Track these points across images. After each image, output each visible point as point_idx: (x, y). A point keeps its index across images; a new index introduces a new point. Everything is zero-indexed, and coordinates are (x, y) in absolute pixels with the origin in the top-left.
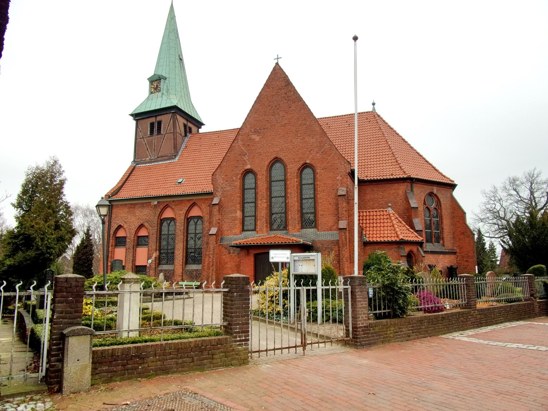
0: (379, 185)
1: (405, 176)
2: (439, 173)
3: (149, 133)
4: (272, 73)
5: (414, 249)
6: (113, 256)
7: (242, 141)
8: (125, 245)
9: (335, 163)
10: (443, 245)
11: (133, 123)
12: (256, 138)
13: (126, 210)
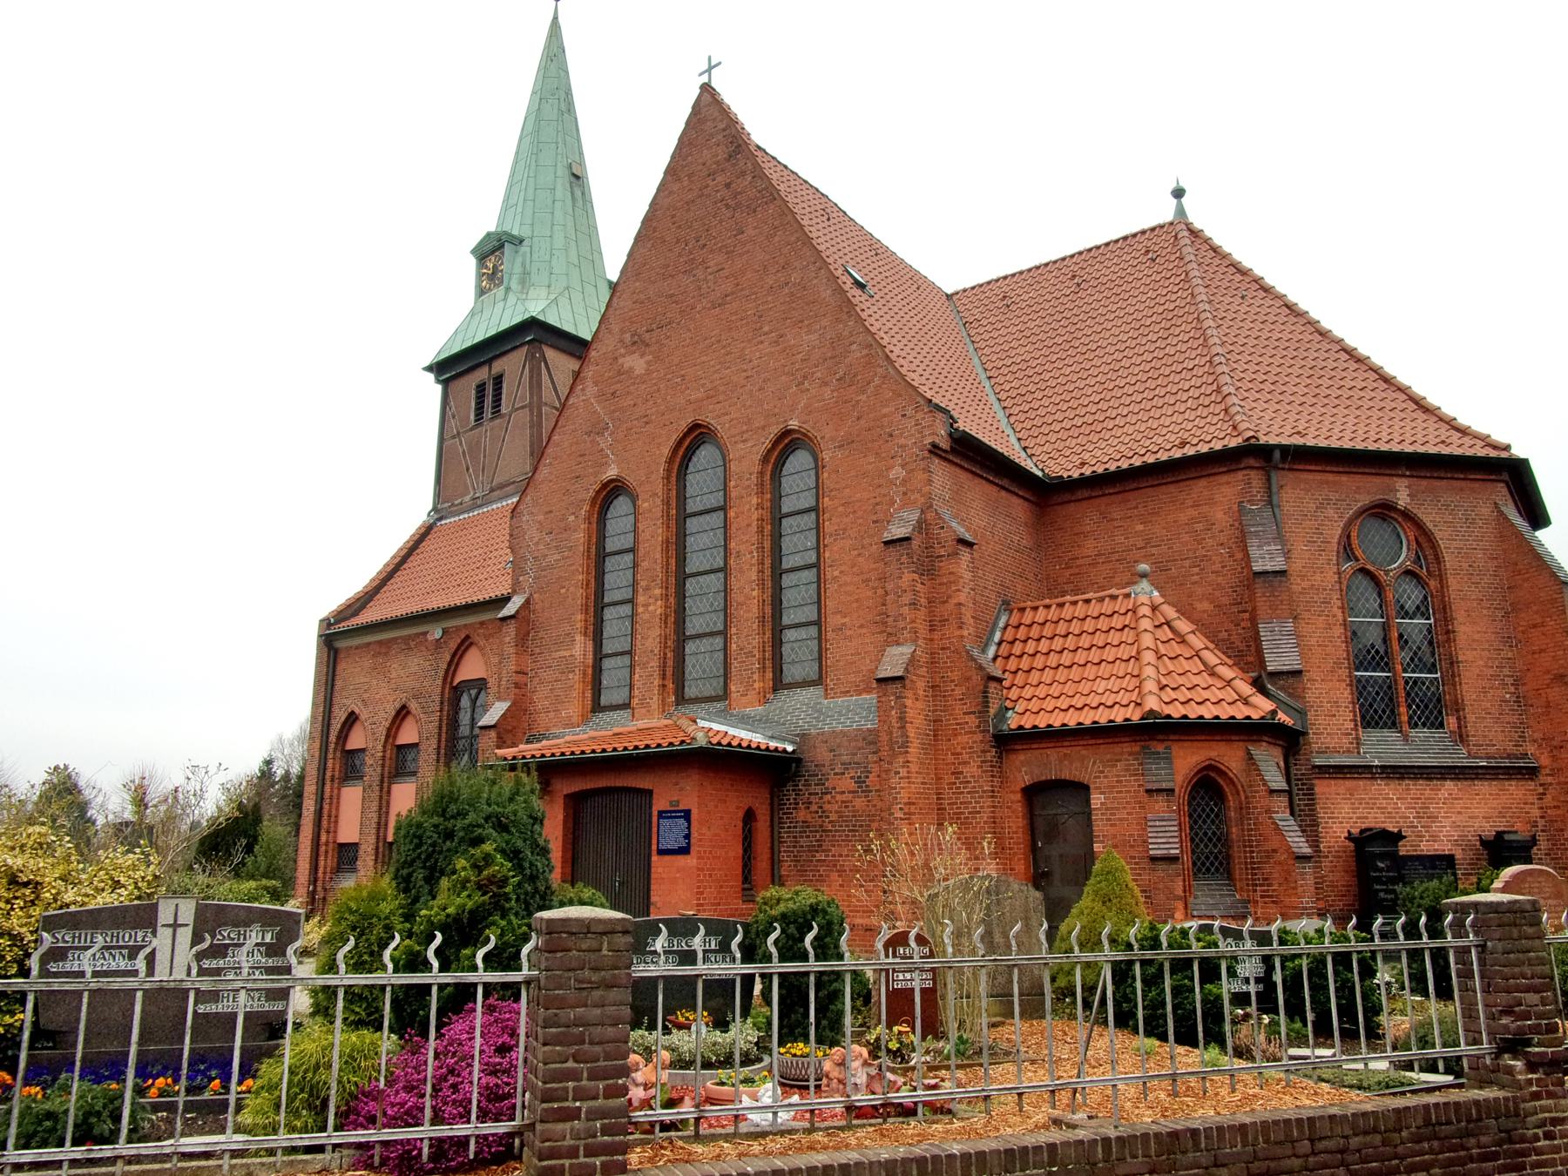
0: (1130, 495)
1: (1233, 443)
2: (1441, 420)
3: (472, 417)
4: (688, 123)
5: (1230, 757)
6: (334, 812)
7: (596, 384)
8: (361, 778)
9: (885, 416)
10: (1461, 736)
11: (432, 391)
12: (636, 363)
13: (367, 662)
